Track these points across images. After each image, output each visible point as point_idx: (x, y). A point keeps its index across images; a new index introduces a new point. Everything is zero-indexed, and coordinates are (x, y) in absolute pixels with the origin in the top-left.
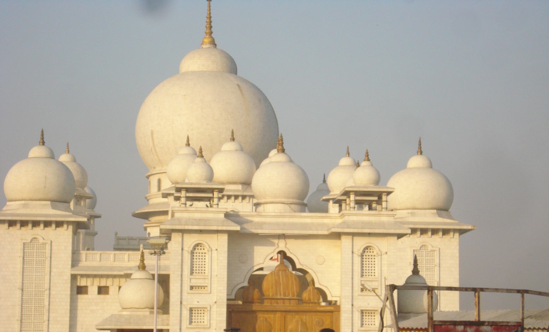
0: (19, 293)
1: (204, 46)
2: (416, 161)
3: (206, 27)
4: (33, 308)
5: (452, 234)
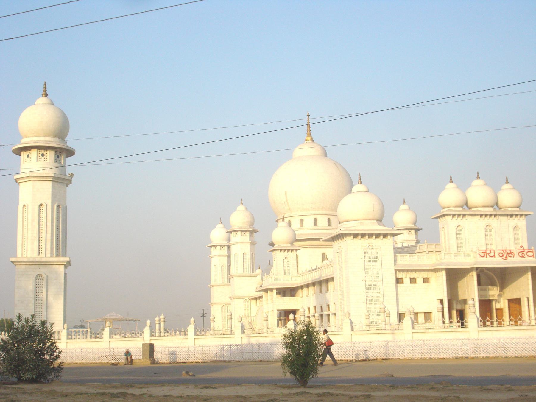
1: (308, 141)
2: (404, 207)
5: (389, 237)
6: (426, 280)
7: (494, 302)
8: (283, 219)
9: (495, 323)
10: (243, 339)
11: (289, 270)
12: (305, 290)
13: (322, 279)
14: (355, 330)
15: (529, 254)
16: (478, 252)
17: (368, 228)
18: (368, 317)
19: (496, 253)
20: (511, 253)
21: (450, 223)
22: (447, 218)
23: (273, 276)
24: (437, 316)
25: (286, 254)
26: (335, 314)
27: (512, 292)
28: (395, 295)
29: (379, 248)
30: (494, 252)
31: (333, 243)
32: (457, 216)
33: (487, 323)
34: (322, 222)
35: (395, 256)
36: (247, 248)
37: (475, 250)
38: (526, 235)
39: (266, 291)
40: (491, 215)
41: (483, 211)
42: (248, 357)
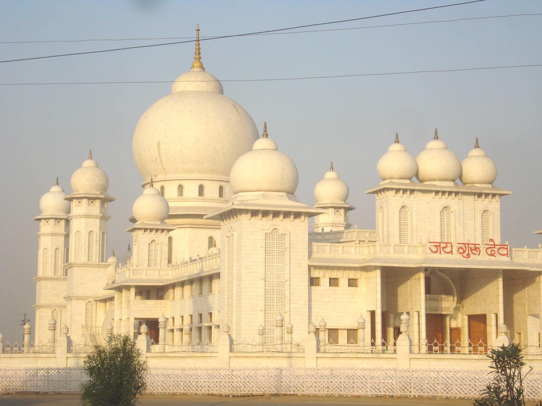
0: (262, 283)
1: (195, 70)
2: (330, 175)
3: (195, 53)
4: (275, 298)
5: (303, 217)
6: (352, 283)
7: (448, 318)
8: (152, 184)
9: (448, 349)
10: (69, 361)
11: (156, 260)
12: (178, 290)
13: (203, 275)
14: (235, 351)
15: (501, 251)
16: (429, 245)
17: (274, 203)
18: (262, 332)
19: (454, 248)
20: (476, 249)
21: (392, 202)
22: (388, 193)
23: (132, 268)
24: (365, 334)
25: (153, 235)
26: (218, 327)
27: (475, 304)
28: (307, 302)
29: (288, 233)
30: (452, 246)
31: (222, 223)
32: (401, 192)
33: (434, 348)
34: (212, 190)
35: (310, 246)
36: (95, 225)
37: (424, 241)
38: (499, 224)
39: (119, 289)
40: (450, 193)
41: (441, 187)
42: (42, 387)
